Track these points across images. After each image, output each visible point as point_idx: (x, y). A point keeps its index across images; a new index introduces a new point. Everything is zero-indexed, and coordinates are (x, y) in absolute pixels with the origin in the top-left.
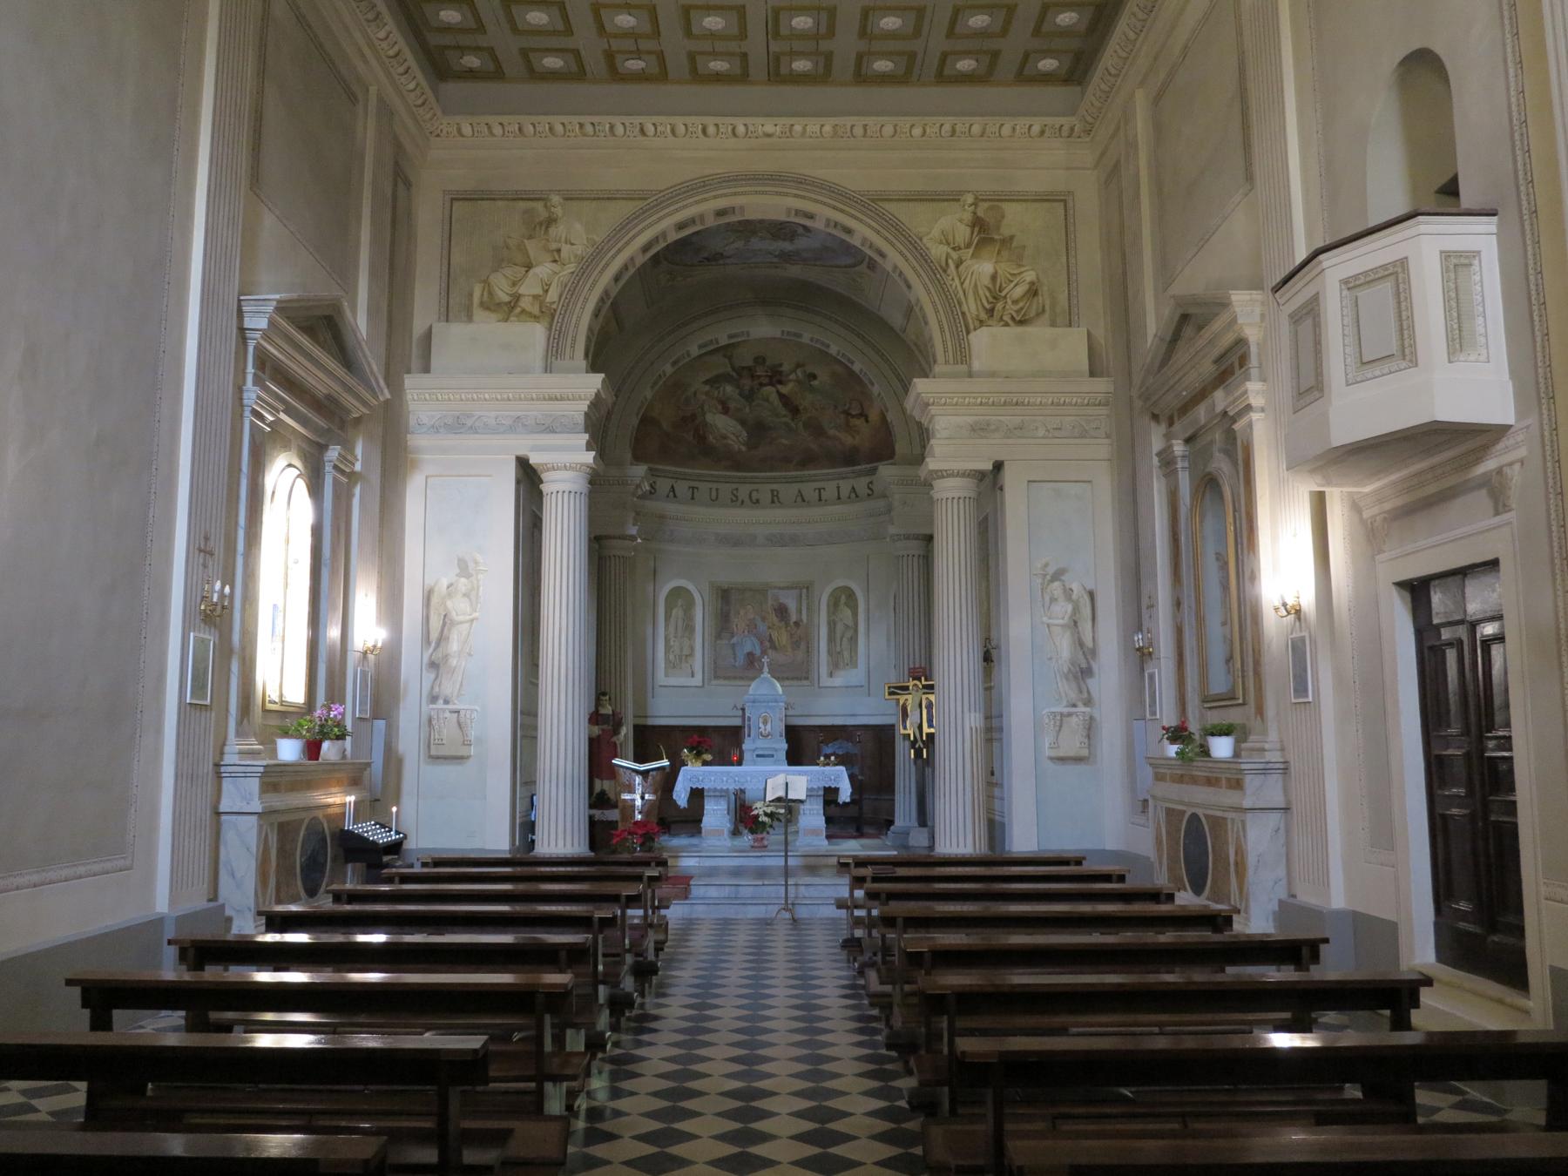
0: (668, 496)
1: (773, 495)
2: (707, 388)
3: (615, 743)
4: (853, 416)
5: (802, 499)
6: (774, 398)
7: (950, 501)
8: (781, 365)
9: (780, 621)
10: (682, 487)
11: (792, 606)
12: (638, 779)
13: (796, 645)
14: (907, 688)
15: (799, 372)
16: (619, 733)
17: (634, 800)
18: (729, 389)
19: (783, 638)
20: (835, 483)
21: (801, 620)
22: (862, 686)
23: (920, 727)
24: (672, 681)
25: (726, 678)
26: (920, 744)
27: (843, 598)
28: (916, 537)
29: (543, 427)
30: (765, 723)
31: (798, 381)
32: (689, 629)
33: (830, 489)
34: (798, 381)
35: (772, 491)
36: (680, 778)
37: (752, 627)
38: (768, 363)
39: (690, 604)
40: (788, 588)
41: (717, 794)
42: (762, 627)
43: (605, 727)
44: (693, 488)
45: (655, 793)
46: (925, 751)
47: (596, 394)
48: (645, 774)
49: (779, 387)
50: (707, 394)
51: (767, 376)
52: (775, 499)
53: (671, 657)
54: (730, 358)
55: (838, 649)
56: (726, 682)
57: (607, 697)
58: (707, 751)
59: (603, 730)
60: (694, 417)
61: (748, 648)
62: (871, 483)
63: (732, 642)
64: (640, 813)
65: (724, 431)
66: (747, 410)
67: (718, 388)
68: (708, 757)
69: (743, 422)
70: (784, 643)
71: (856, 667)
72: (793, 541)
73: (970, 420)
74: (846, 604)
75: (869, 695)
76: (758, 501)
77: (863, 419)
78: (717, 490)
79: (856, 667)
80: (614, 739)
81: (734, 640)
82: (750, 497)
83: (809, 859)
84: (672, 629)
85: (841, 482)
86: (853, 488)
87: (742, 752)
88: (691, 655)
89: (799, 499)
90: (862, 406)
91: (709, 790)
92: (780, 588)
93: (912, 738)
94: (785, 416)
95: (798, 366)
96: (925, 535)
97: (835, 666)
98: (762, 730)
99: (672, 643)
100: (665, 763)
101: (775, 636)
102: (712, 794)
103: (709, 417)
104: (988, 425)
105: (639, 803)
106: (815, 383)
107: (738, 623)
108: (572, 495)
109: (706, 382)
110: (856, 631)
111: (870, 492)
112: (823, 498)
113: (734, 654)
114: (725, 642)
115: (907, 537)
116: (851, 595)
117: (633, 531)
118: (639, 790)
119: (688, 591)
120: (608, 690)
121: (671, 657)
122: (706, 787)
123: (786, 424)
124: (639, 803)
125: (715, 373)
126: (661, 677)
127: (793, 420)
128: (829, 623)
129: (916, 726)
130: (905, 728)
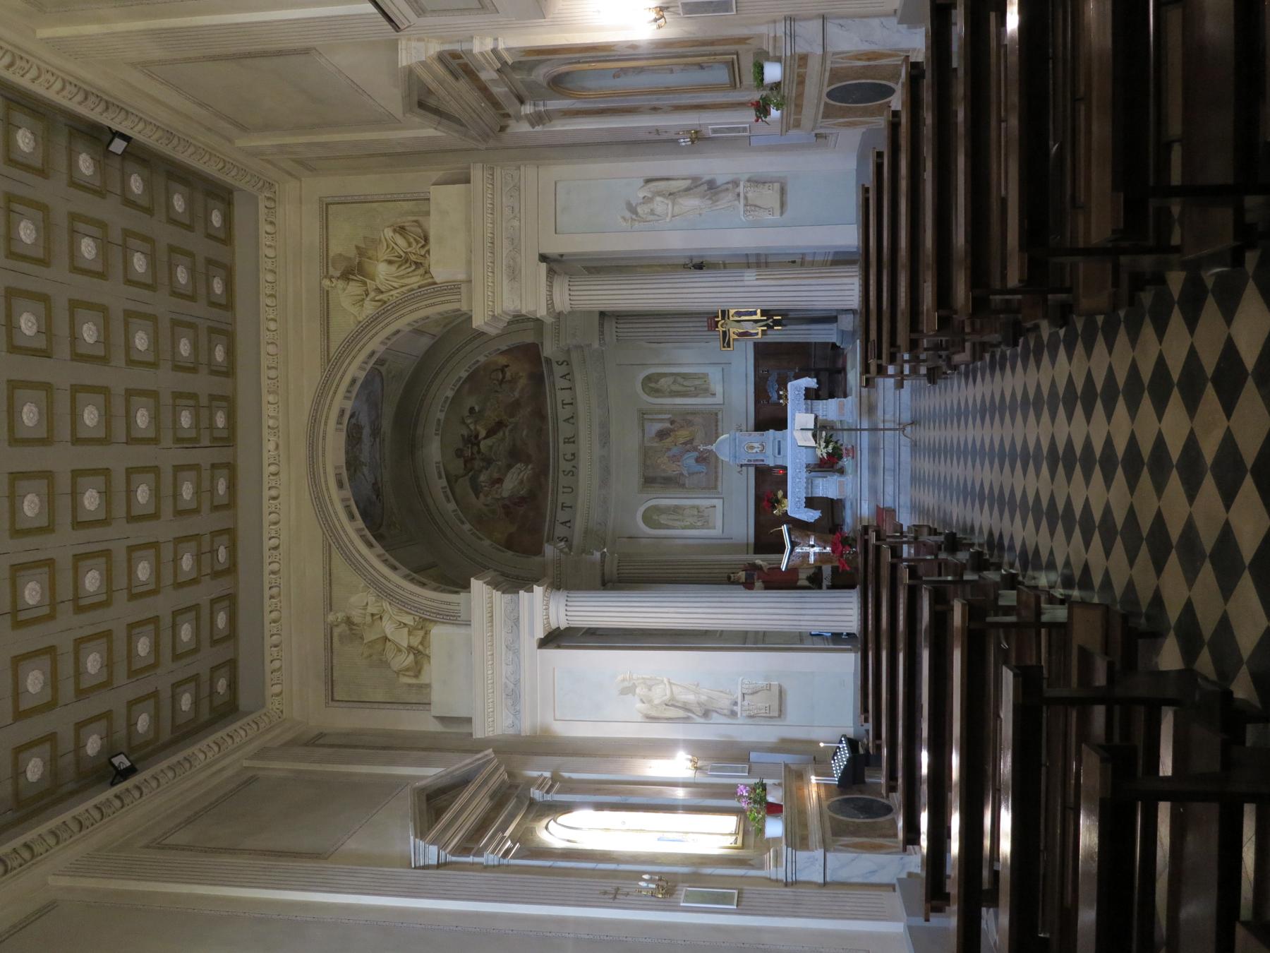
1: (569, 442)
2: (481, 495)
3: (769, 569)
4: (504, 378)
5: (571, 419)
6: (489, 442)
7: (572, 298)
8: (463, 436)
10: (562, 516)
11: (658, 426)
12: (798, 550)
14: (724, 333)
15: (469, 421)
17: (815, 553)
18: (482, 478)
21: (669, 419)
22: (723, 369)
23: (756, 321)
24: (719, 523)
26: (769, 322)
27: (652, 385)
28: (601, 325)
30: (752, 448)
31: (476, 423)
32: (676, 510)
33: (562, 396)
34: (476, 423)
35: (565, 443)
37: (675, 459)
39: (657, 509)
41: (810, 487)
42: (675, 450)
43: (756, 577)
44: (563, 507)
45: (809, 536)
48: (794, 545)
49: (480, 438)
50: (486, 496)
51: (472, 448)
52: (571, 440)
55: (693, 389)
56: (720, 479)
57: (732, 575)
58: (776, 495)
59: (758, 579)
60: (505, 507)
61: (692, 461)
62: (557, 362)
64: (825, 548)
66: (500, 463)
68: (780, 494)
69: (510, 467)
72: (605, 426)
74: (657, 382)
76: (573, 455)
78: (564, 487)
80: (765, 570)
81: (685, 473)
84: (677, 524)
86: (562, 377)
88: (697, 508)
89: (571, 421)
90: (494, 371)
91: (807, 493)
92: (643, 436)
93: (765, 328)
94: (504, 433)
95: (463, 422)
97: (706, 391)
98: (758, 450)
99: (688, 523)
101: (682, 440)
103: (506, 494)
105: (817, 549)
106: (477, 409)
107: (671, 469)
112: (570, 402)
114: (687, 482)
115: (602, 333)
116: (649, 379)
117: (597, 555)
118: (806, 549)
121: (699, 524)
122: (805, 495)
123: (511, 431)
124: (817, 549)
127: (506, 426)
128: (671, 396)
129: (755, 325)
130: (757, 334)
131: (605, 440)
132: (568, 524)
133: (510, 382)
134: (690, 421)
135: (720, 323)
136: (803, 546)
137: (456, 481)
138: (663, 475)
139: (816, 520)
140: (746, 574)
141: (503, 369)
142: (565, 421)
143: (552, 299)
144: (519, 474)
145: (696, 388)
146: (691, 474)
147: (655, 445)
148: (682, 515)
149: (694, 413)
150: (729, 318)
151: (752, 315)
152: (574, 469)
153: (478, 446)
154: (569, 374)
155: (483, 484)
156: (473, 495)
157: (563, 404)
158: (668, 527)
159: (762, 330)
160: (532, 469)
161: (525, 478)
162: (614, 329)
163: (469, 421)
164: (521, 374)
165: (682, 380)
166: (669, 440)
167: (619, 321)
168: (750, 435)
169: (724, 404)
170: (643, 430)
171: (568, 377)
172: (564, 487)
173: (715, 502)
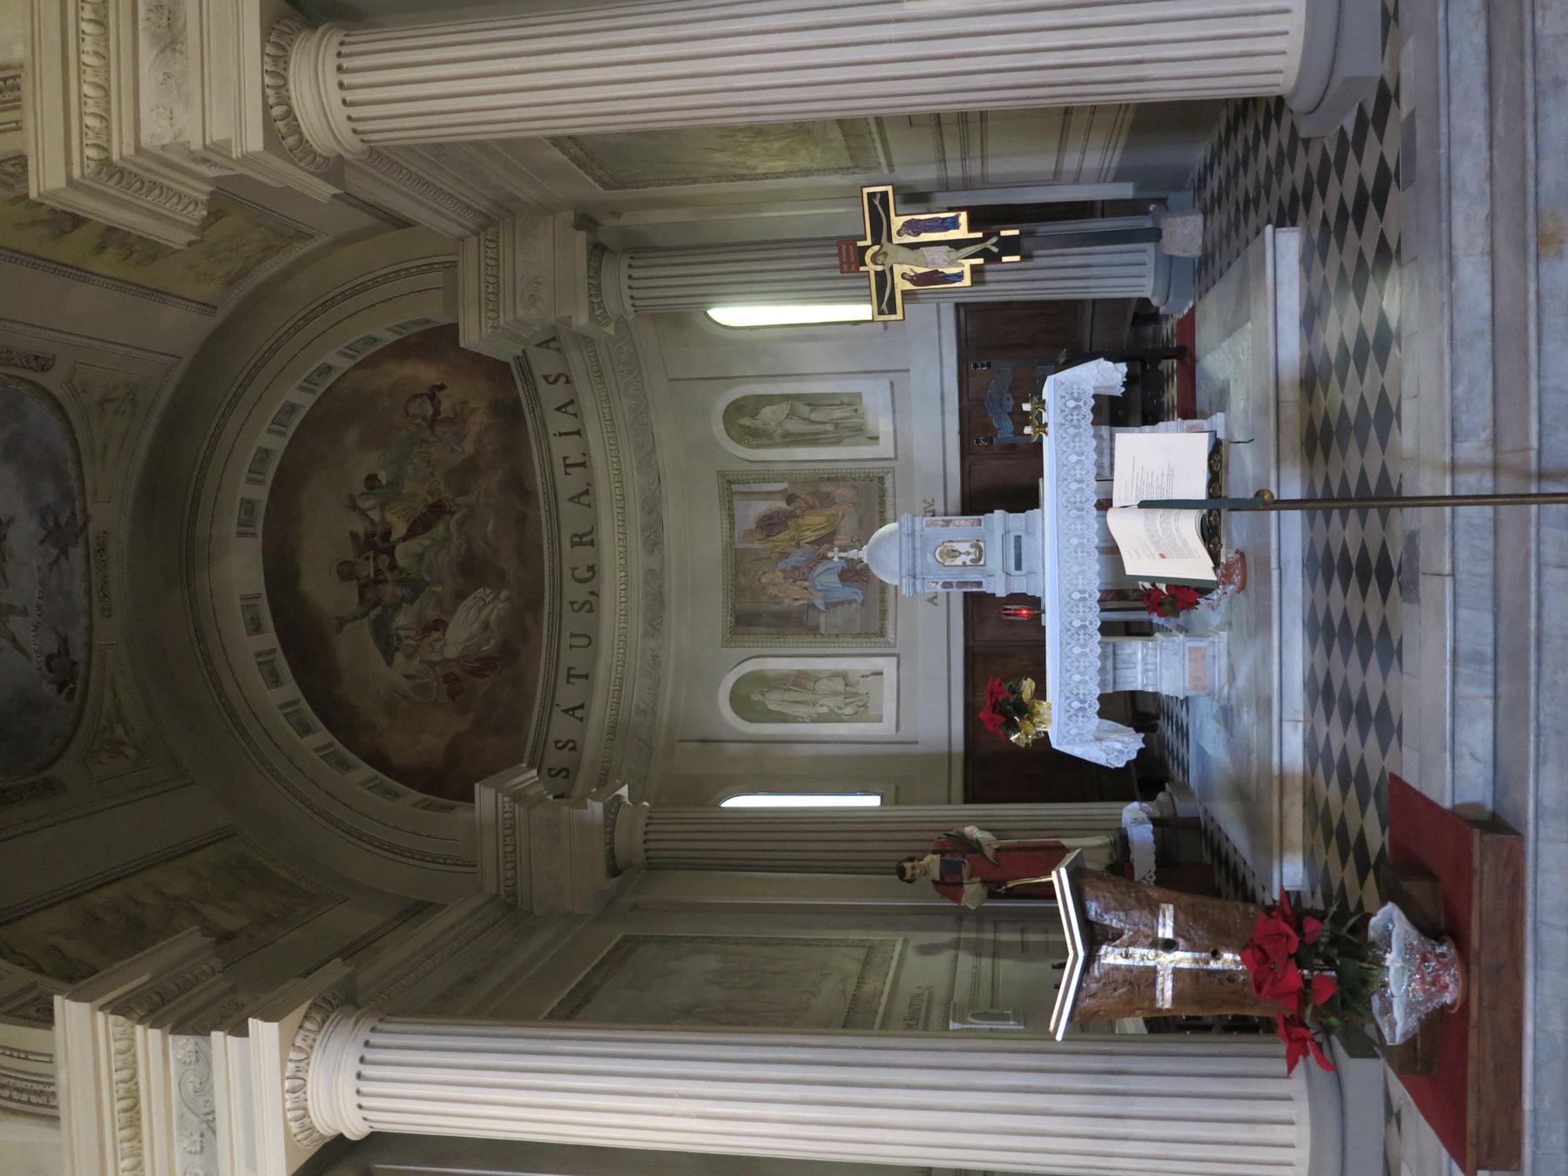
0: (581, 719)
1: (581, 544)
2: (399, 658)
3: (997, 850)
4: (437, 412)
5: (585, 496)
6: (415, 545)
7: (351, 96)
8: (354, 535)
9: (787, 527)
10: (568, 695)
11: (761, 508)
12: (1111, 957)
13: (826, 500)
14: (881, 276)
15: (366, 504)
16: (977, 841)
17: (1177, 973)
18: (401, 620)
19: (815, 521)
20: (553, 440)
21: (784, 491)
22: (892, 384)
23: (957, 245)
24: (889, 709)
25: (883, 613)
26: (990, 244)
27: (746, 421)
28: (594, 272)
29: (208, 1133)
30: (954, 554)
31: (383, 506)
32: (799, 681)
33: (563, 448)
34: (383, 506)
35: (573, 545)
36: (1077, 751)
37: (799, 574)
38: (350, 557)
39: (761, 680)
40: (731, 516)
41: (1109, 664)
42: (797, 558)
43: (965, 871)
44: (569, 676)
45: (1154, 910)
46: (1003, 233)
47: (114, 1013)
48: (1095, 936)
49: (394, 537)
50: (409, 657)
51: (375, 559)
52: (586, 540)
53: (848, 711)
54: (342, 622)
55: (829, 427)
56: (890, 615)
57: (908, 865)
58: (1016, 691)
59: (971, 876)
60: (450, 679)
61: (832, 580)
62: (546, 378)
63: (822, 608)
64: (1215, 955)
65: (476, 626)
66: (439, 589)
67: (399, 639)
68: (1028, 686)
69: (460, 596)
70: (822, 519)
71: (859, 395)
72: (652, 506)
73: (147, 54)
74: (754, 415)
75: (907, 371)
77: (440, 395)
78: (572, 636)
79: (859, 395)
80: (989, 853)
81: (819, 603)
82: (582, 581)
83: (1285, 446)
84: (801, 710)
85: (552, 430)
86: (558, 409)
87: (1016, 598)
88: (843, 675)
89: (584, 499)
90: (414, 397)
91: (1102, 684)
92: (732, 529)
93: (980, 261)
94: (447, 528)
95: (354, 507)
96: (590, 253)
97: (859, 432)
98: (967, 559)
99: (824, 710)
100: (1060, 878)
101: (811, 536)
102: (1110, 677)
103: (451, 652)
104: (159, 7)
105: (1183, 958)
106: (383, 477)
107: (791, 596)
108: (368, 1071)
109: (389, 660)
110: (798, 397)
111: (563, 379)
112: (580, 460)
113: (842, 603)
114: (822, 620)
115: (595, 289)
116: (737, 409)
117: (596, 808)
118: (1141, 956)
119: (737, 683)
120: (894, 864)
121: (848, 711)
122: (1098, 692)
123: (462, 523)
124: (1183, 958)
125: (371, 645)
126: (883, 729)
127: (453, 513)
128: (787, 445)
129: (954, 254)
130: (960, 276)
131: (654, 540)
132: (578, 713)
133: (451, 421)
134: (828, 495)
135: (869, 253)
136: (1133, 943)
137: (340, 628)
138: (775, 607)
139: (1128, 763)
140: (943, 862)
141: (433, 394)
142: (571, 500)
143: (285, 101)
144: (480, 611)
145: (837, 426)
146: (831, 606)
147: (757, 545)
148: (814, 692)
149: (834, 479)
150: (890, 239)
151: (947, 229)
152: (590, 598)
153: (392, 555)
154: (572, 402)
155: (402, 633)
156: (380, 657)
157: (567, 466)
158: (783, 718)
159: (973, 267)
160: (508, 599)
161: (493, 616)
162: (625, 282)
163: (366, 505)
164: (473, 404)
165: (808, 409)
166: (784, 535)
167: (637, 263)
168: (947, 523)
169: (896, 458)
170: (731, 516)
171: (570, 409)
172: (572, 636)
173: (878, 663)
